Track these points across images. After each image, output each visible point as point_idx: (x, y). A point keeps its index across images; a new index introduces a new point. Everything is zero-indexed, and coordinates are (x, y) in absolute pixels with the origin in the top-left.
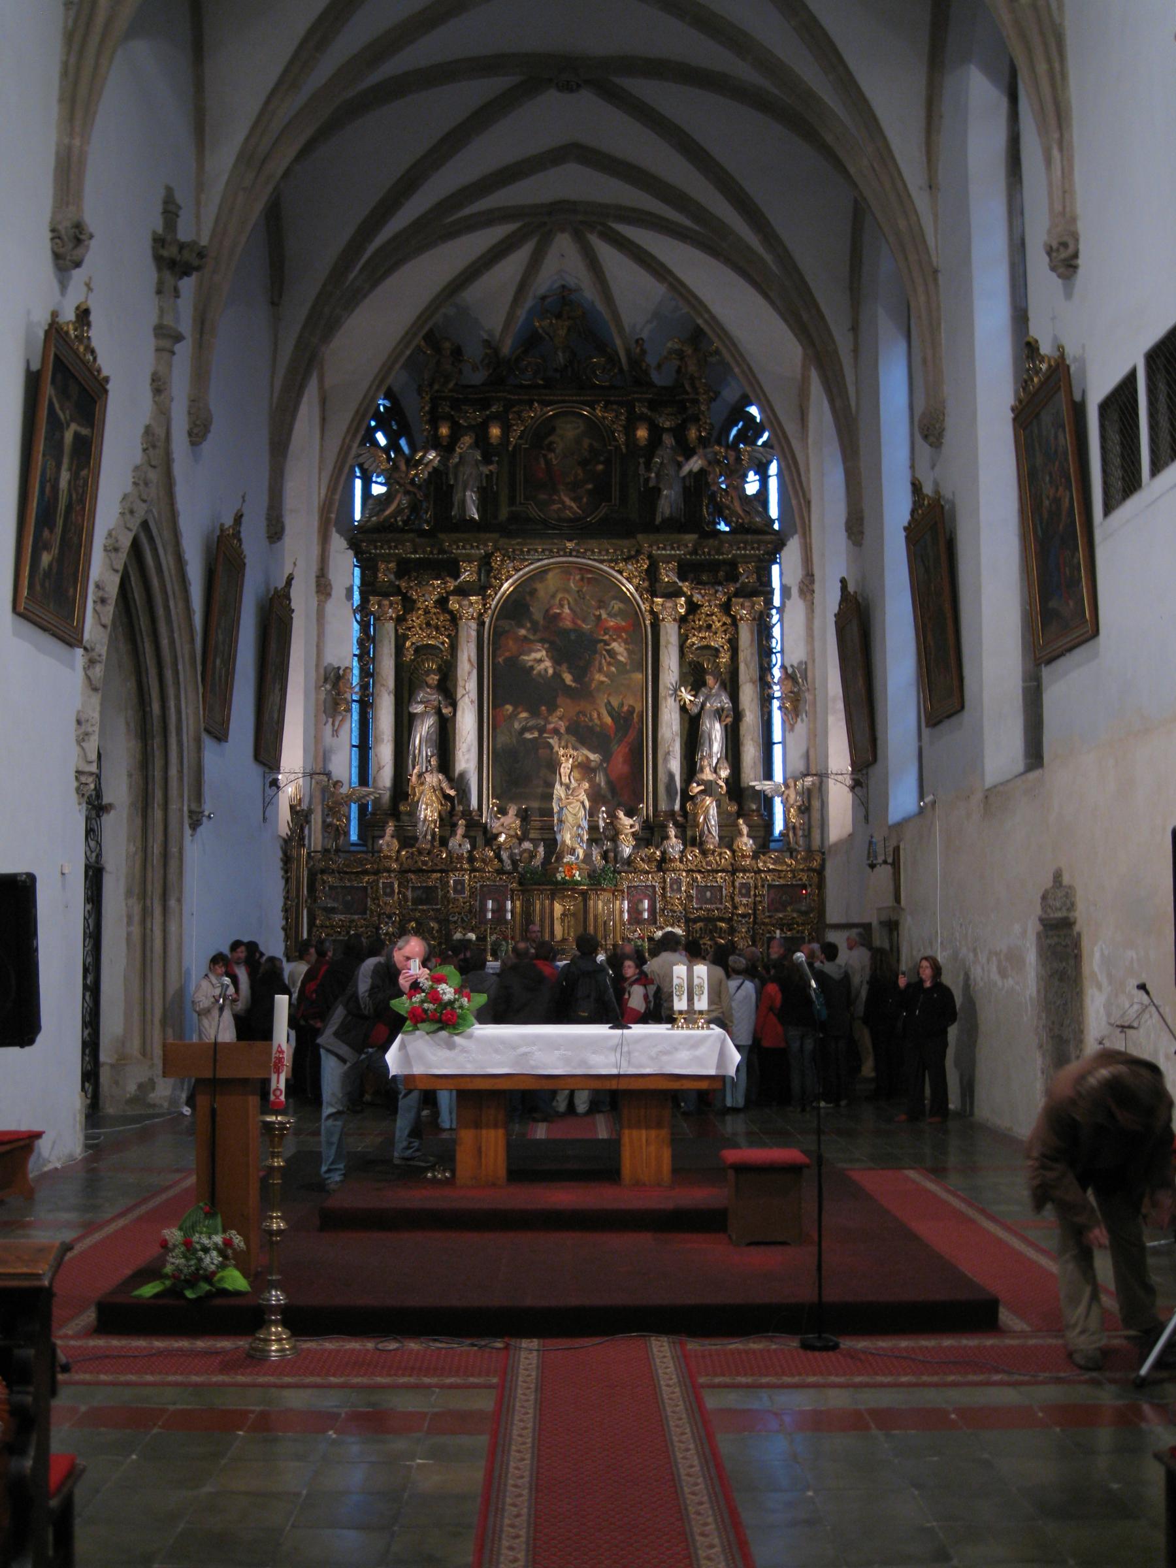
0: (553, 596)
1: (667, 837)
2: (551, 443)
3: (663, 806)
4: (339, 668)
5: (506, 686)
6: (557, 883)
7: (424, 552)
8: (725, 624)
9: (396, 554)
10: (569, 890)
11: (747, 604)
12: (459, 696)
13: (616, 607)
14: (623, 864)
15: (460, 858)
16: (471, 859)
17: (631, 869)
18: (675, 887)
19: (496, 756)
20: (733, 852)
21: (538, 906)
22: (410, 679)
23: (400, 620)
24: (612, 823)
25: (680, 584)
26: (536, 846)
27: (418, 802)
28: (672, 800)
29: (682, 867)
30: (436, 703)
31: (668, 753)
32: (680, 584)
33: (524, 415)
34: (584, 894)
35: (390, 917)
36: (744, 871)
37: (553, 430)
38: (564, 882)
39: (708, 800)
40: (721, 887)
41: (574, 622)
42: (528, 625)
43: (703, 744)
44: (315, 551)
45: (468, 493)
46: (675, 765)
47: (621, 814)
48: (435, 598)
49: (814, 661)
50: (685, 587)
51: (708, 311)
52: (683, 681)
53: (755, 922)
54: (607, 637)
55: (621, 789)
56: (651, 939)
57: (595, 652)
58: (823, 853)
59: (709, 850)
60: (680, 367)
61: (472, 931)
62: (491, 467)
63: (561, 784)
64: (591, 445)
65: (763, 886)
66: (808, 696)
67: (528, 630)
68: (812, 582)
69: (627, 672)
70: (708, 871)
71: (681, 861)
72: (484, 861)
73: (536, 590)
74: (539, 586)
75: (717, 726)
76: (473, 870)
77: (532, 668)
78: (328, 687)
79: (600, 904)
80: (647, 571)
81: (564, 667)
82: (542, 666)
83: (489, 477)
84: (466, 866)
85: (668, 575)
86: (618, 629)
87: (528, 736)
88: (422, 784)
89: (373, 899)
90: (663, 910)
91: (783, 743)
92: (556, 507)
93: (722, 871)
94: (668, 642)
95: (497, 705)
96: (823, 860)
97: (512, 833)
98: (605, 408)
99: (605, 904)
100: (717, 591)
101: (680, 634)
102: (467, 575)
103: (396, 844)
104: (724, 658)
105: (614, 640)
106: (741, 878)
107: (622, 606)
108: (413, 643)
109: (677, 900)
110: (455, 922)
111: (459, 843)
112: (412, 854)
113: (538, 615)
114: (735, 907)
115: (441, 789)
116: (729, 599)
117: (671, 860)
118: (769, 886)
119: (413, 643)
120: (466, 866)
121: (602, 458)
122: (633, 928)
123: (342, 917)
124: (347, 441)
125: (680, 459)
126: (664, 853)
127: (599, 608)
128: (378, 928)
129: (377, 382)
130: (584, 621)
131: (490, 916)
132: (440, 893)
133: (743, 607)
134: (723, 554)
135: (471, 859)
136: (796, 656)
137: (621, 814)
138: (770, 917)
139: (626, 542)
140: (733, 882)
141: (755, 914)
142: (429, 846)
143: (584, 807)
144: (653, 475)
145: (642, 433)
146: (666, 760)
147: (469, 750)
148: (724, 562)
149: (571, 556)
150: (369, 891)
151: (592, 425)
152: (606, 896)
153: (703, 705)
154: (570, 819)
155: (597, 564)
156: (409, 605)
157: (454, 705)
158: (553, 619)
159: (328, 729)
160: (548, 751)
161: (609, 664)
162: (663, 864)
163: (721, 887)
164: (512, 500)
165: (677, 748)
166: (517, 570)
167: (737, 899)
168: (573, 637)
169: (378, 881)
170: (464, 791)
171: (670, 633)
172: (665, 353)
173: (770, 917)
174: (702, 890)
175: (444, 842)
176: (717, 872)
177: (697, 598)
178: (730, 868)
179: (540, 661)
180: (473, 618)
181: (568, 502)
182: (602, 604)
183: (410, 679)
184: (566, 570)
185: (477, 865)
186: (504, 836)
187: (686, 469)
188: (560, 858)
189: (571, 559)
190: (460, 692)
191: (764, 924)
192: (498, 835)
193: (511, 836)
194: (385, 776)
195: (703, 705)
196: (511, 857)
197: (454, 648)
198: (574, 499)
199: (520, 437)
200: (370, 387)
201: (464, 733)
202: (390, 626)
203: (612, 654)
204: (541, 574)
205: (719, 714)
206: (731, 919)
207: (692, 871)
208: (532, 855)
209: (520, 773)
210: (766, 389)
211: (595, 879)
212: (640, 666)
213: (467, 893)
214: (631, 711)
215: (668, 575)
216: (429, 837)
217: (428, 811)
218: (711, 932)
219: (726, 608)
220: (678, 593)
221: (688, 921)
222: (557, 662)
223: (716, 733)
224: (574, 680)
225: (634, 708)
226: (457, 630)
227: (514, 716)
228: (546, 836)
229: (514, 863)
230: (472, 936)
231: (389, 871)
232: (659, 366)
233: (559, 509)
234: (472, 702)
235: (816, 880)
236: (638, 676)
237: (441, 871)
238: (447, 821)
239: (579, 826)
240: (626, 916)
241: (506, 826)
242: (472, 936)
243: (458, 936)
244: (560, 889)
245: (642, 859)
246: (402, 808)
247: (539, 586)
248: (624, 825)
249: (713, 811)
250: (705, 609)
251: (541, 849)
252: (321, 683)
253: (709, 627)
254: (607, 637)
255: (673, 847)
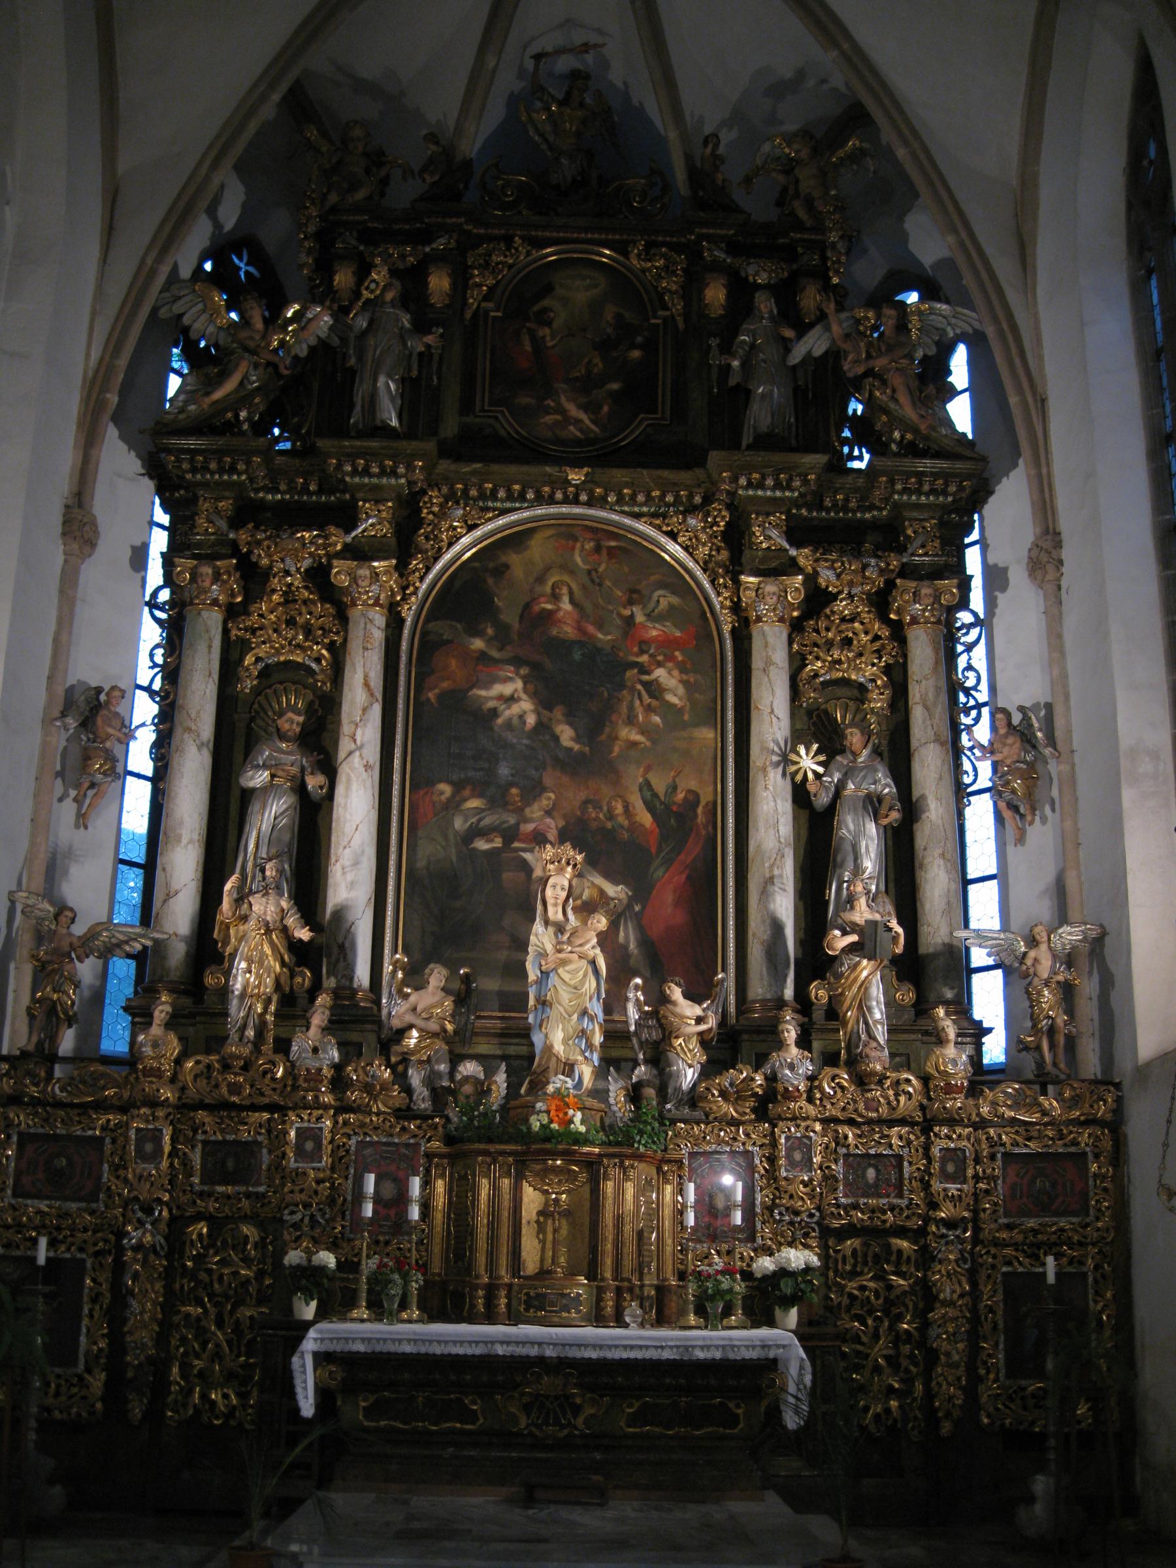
0: (541, 580)
1: (780, 1045)
2: (545, 310)
3: (758, 989)
4: (99, 690)
5: (434, 735)
6: (527, 1137)
7: (291, 490)
8: (876, 638)
9: (234, 483)
10: (555, 1154)
11: (925, 591)
12: (342, 754)
13: (664, 603)
14: (679, 1104)
15: (314, 1078)
16: (339, 1082)
17: (698, 1114)
18: (798, 1156)
19: (414, 882)
20: (925, 1079)
21: (484, 1193)
22: (249, 727)
23: (232, 612)
24: (655, 1014)
25: (793, 552)
26: (490, 1072)
27: (233, 956)
28: (778, 978)
29: (811, 1110)
30: (295, 770)
31: (771, 880)
32: (793, 552)
33: (497, 258)
34: (593, 1166)
35: (148, 1211)
36: (952, 1121)
37: (548, 289)
38: (547, 1135)
39: (866, 968)
40: (899, 1158)
41: (580, 629)
42: (490, 631)
43: (842, 865)
44: (66, 458)
45: (382, 380)
46: (784, 905)
47: (676, 993)
48: (306, 564)
49: (1067, 697)
50: (804, 556)
51: (848, 37)
52: (798, 737)
53: (976, 1240)
54: (644, 658)
55: (677, 937)
56: (747, 1275)
57: (622, 686)
58: (1118, 1086)
59: (873, 1073)
60: (785, 190)
61: (333, 1247)
62: (429, 339)
63: (547, 922)
64: (619, 317)
65: (992, 1157)
66: (1053, 767)
67: (489, 641)
68: (1058, 545)
69: (684, 726)
70: (870, 1122)
71: (810, 1100)
72: (368, 1088)
73: (507, 567)
74: (514, 559)
75: (872, 828)
76: (343, 1108)
77: (494, 713)
78: (72, 722)
79: (630, 1189)
80: (724, 534)
81: (558, 713)
82: (515, 709)
83: (424, 358)
84: (327, 1099)
85: (767, 536)
86: (668, 644)
87: (482, 845)
88: (244, 919)
89: (115, 1168)
90: (770, 1209)
91: (1001, 876)
92: (549, 419)
93: (902, 1122)
94: (769, 662)
95: (420, 781)
96: (1119, 1100)
97: (433, 1026)
98: (648, 253)
99: (640, 1191)
100: (865, 567)
101: (791, 656)
102: (373, 523)
103: (173, 1046)
104: (878, 701)
105: (659, 665)
106: (943, 1140)
107: (675, 600)
108: (258, 659)
109: (799, 1182)
110: (296, 1226)
111: (315, 1045)
112: (209, 1067)
113: (510, 617)
114: (934, 1206)
115: (285, 930)
116: (890, 585)
117: (788, 1096)
118: (1005, 1155)
119: (258, 659)
120: (327, 1099)
121: (639, 339)
122: (702, 1248)
123: (43, 1206)
124: (149, 261)
125: (789, 333)
126: (772, 1079)
127: (631, 602)
128: (121, 1234)
129: (213, 154)
130: (600, 626)
131: (368, 1210)
132: (266, 1158)
133: (916, 597)
134: (872, 507)
135: (339, 1082)
136: (1026, 689)
137: (676, 993)
138: (1009, 1227)
139: (685, 476)
140: (927, 1148)
141: (975, 1220)
142: (246, 1051)
143: (596, 972)
144: (736, 363)
145: (716, 294)
146: (765, 894)
147: (356, 863)
148: (874, 525)
149: (576, 502)
150: (108, 1147)
151: (621, 284)
152: (644, 1170)
153: (840, 788)
154: (565, 995)
155: (628, 521)
156: (254, 579)
157: (329, 770)
158: (538, 621)
159: (68, 809)
160: (522, 875)
161: (649, 709)
162: (768, 1104)
163: (899, 1158)
164: (467, 406)
165: (787, 871)
166: (471, 528)
167: (937, 1186)
168: (577, 656)
169: (127, 1125)
170: (342, 947)
171: (772, 646)
172: (759, 162)
173: (1009, 1227)
174: (857, 1163)
175: (283, 1046)
176: (891, 1123)
177: (826, 577)
178: (918, 1116)
179: (511, 699)
180: (377, 603)
181: (574, 411)
182: (635, 596)
183: (249, 727)
184: (568, 531)
185: (353, 1096)
186: (415, 1033)
187: (798, 354)
188: (538, 1085)
189: (577, 510)
190: (345, 745)
191: (996, 1243)
192: (402, 1033)
193: (435, 1035)
194: (180, 913)
195: (840, 788)
196: (430, 1082)
197: (339, 655)
198: (585, 408)
199: (486, 298)
200: (200, 163)
201: (348, 828)
202: (213, 619)
203: (655, 690)
204: (516, 540)
205: (873, 805)
206: (922, 1232)
207: (836, 1120)
208: (482, 1089)
209: (462, 913)
210: (960, 196)
211: (621, 1142)
212: (713, 717)
213: (326, 1160)
214: (693, 800)
215: (767, 536)
216: (250, 1033)
217: (252, 973)
218: (877, 1259)
219: (881, 602)
220: (792, 567)
221: (826, 1232)
222: (544, 703)
223: (866, 843)
224: (577, 739)
225: (697, 795)
226: (346, 631)
227: (453, 805)
228: (512, 1050)
229: (439, 1096)
230: (328, 1259)
231: (154, 1103)
232: (748, 180)
233: (556, 422)
234: (367, 767)
235: (1107, 1144)
236: (707, 734)
237: (271, 1108)
238: (291, 1006)
239: (584, 1012)
240: (691, 1219)
241: (421, 1009)
242: (328, 1259)
243: (294, 1257)
244: (533, 1151)
245: (723, 1094)
246: (209, 980)
247: (514, 559)
248: (682, 1017)
249: (877, 992)
250: (842, 606)
251: (501, 1078)
252: (57, 714)
253: (847, 642)
254: (644, 658)
255: (792, 1067)
